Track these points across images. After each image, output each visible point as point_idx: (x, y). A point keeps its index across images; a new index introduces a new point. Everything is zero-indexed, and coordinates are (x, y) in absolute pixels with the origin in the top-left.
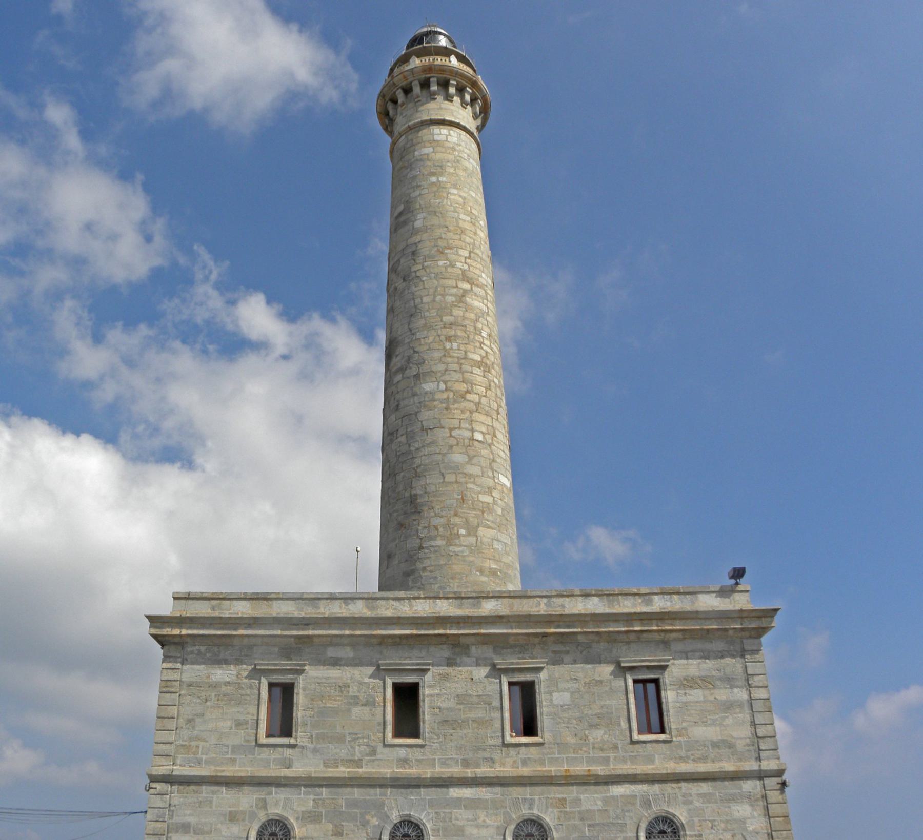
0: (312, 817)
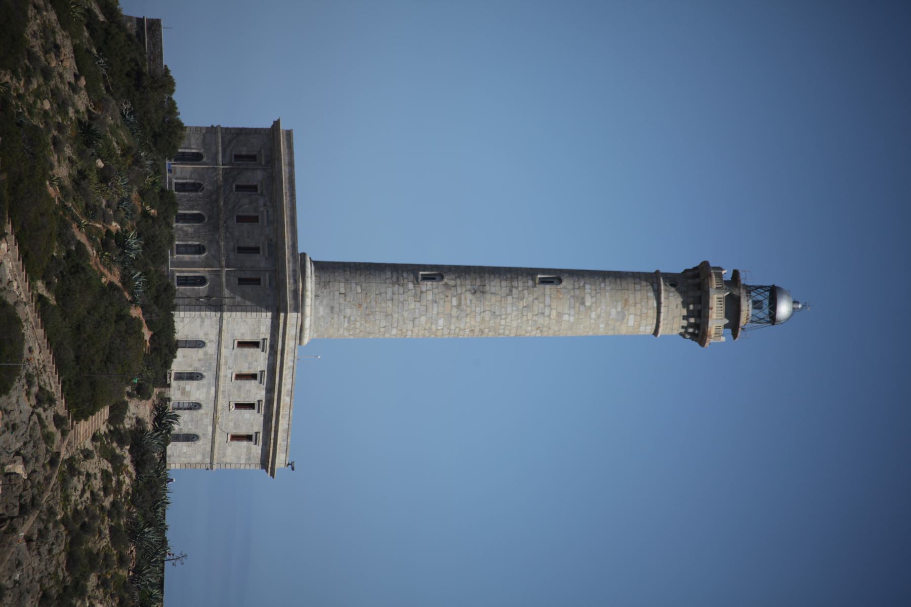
0: (206, 354)
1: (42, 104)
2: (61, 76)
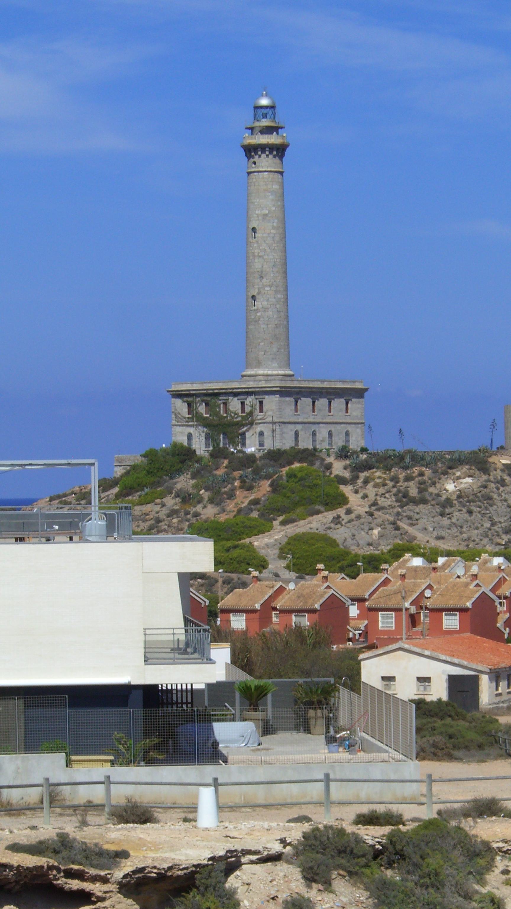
0: (302, 430)
1: (174, 523)
2: (157, 513)
